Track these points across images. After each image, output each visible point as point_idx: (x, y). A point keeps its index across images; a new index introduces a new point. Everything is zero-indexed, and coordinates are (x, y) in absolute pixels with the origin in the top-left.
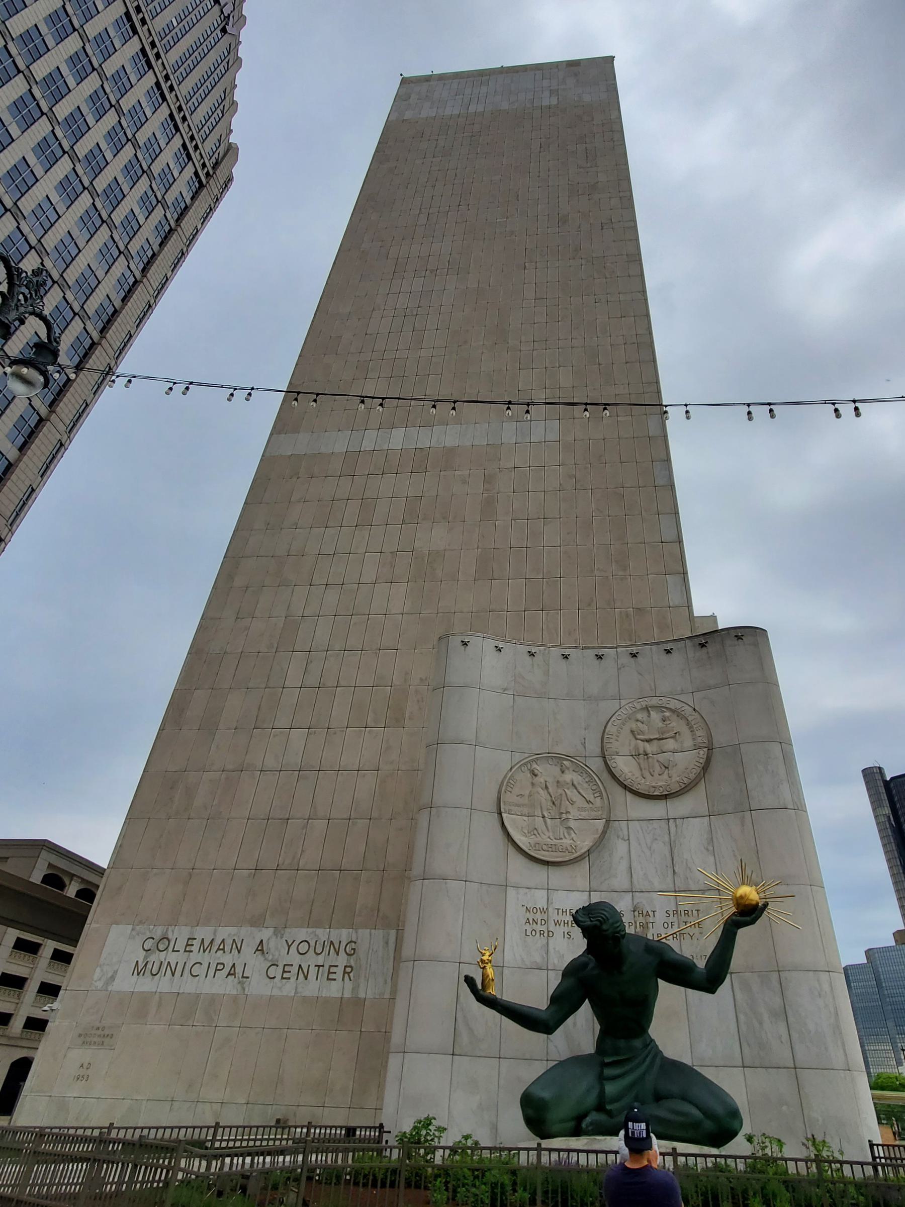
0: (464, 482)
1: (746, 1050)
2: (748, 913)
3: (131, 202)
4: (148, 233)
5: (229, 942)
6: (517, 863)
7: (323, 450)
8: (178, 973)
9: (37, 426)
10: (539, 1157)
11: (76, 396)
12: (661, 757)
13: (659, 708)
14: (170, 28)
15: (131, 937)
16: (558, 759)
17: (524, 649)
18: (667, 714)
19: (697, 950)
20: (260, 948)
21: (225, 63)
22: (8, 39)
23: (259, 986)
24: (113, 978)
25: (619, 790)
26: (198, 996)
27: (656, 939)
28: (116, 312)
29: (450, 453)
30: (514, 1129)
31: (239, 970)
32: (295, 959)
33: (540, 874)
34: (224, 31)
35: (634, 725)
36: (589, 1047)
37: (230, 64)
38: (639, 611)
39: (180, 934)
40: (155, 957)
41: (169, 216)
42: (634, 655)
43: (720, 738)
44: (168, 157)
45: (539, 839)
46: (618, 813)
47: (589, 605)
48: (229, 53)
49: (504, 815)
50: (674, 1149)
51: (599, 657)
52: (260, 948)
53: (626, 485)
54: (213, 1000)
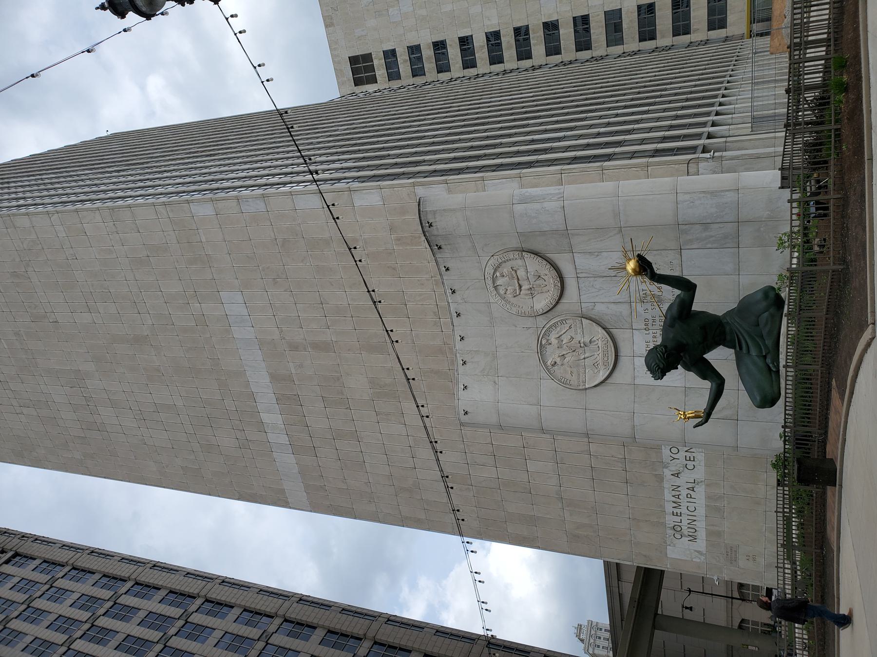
1: (728, 245)
2: (644, 267)
3: (64, 609)
4: (86, 587)
5: (674, 493)
6: (617, 377)
7: (296, 470)
8: (694, 518)
9: (292, 622)
12: (532, 279)
16: (541, 349)
17: (461, 369)
18: (498, 274)
19: (670, 294)
20: (677, 475)
23: (700, 473)
25: (559, 307)
26: (707, 506)
29: (275, 378)
30: (777, 414)
31: (690, 485)
32: (682, 454)
33: (624, 361)
38: (392, 229)
39: (670, 520)
40: (685, 531)
41: (61, 574)
43: (515, 243)
47: (394, 269)
49: (587, 386)
52: (677, 475)
53: (273, 237)
54: (709, 497)
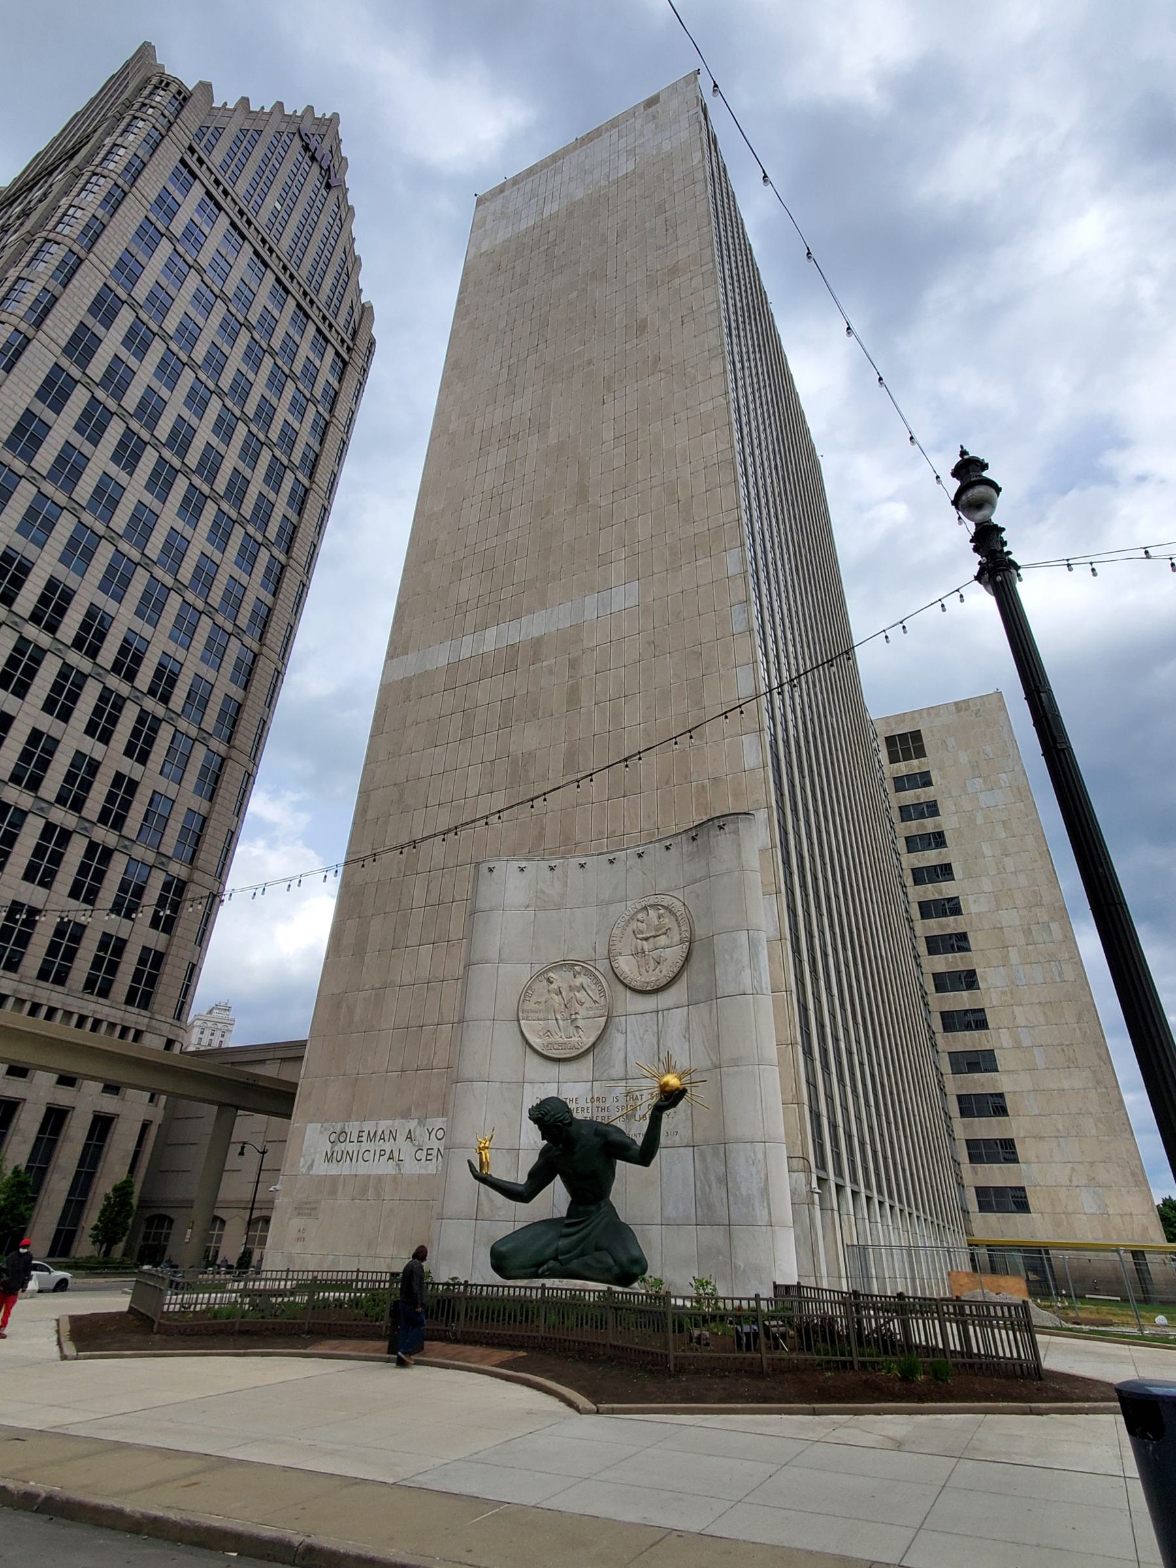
0: (551, 672)
2: (670, 1098)
4: (305, 436)
6: (533, 1061)
7: (429, 667)
10: (465, 1289)
11: (280, 623)
13: (655, 906)
14: (275, 213)
15: (321, 1133)
16: (568, 965)
20: (409, 1137)
21: (337, 220)
22: (175, 241)
23: (411, 1167)
24: (312, 1165)
25: (621, 988)
27: (606, 1122)
28: (295, 528)
29: (538, 642)
30: (483, 1275)
31: (396, 1155)
33: (552, 1070)
34: (328, 186)
35: (634, 925)
36: (562, 1210)
37: (343, 217)
40: (339, 1147)
42: (640, 856)
43: (700, 932)
44: (305, 350)
45: (552, 1040)
46: (619, 1009)
47: (667, 783)
48: (339, 208)
49: (522, 1022)
50: (543, 1285)
51: (611, 862)
52: (409, 1137)
54: (380, 1178)
